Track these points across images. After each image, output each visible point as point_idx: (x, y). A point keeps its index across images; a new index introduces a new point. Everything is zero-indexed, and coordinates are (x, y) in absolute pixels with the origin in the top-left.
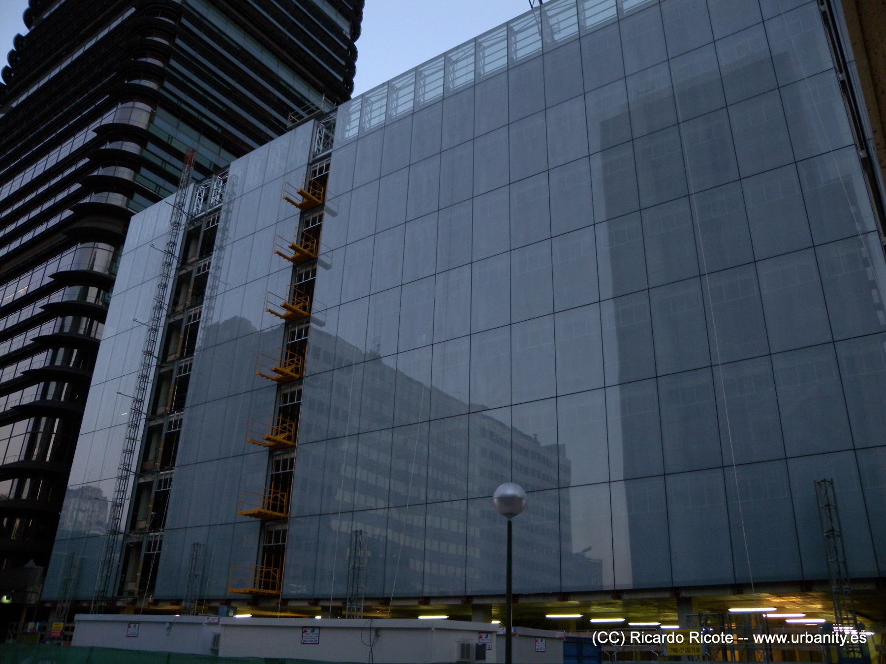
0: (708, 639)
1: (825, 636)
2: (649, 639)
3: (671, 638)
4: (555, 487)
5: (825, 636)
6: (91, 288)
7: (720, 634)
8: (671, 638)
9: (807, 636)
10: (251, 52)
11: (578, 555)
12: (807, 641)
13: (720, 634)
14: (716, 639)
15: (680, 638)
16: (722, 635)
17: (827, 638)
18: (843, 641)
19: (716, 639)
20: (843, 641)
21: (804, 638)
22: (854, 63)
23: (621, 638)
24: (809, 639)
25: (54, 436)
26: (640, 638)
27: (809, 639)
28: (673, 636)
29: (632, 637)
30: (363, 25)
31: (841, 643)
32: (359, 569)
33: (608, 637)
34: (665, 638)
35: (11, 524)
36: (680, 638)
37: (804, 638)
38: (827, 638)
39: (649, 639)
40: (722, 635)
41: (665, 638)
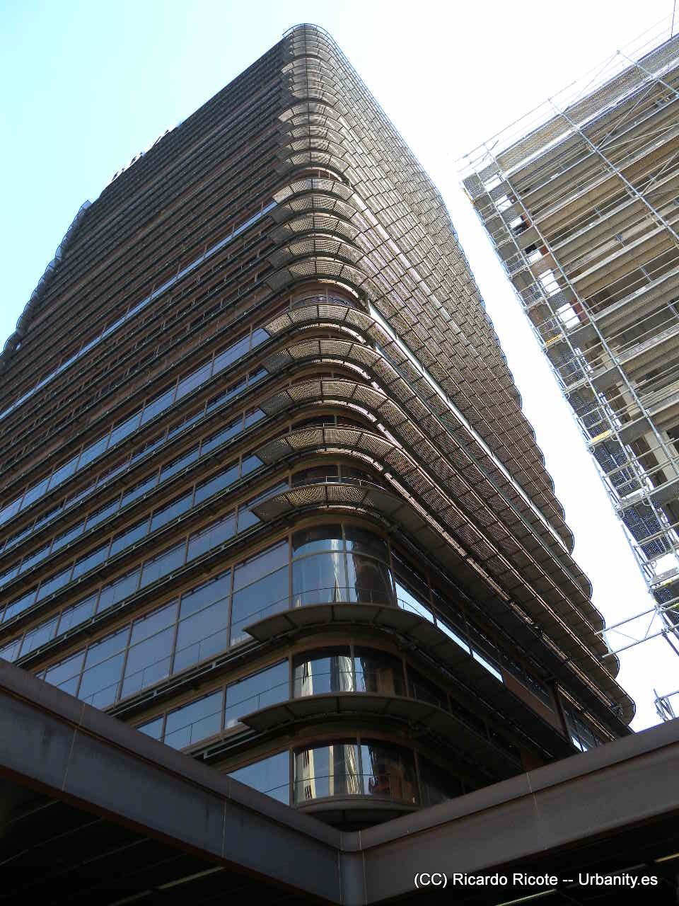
5: (615, 878)
6: (362, 687)
9: (597, 878)
10: (480, 281)
11: (285, 122)
12: (597, 883)
15: (503, 881)
16: (547, 877)
17: (617, 879)
18: (634, 883)
19: (437, 879)
20: (634, 883)
21: (594, 880)
31: (632, 885)
32: (73, 728)
33: (430, 879)
34: (489, 880)
36: (503, 881)
37: (594, 880)
38: (617, 879)
40: (547, 877)
41: (489, 880)
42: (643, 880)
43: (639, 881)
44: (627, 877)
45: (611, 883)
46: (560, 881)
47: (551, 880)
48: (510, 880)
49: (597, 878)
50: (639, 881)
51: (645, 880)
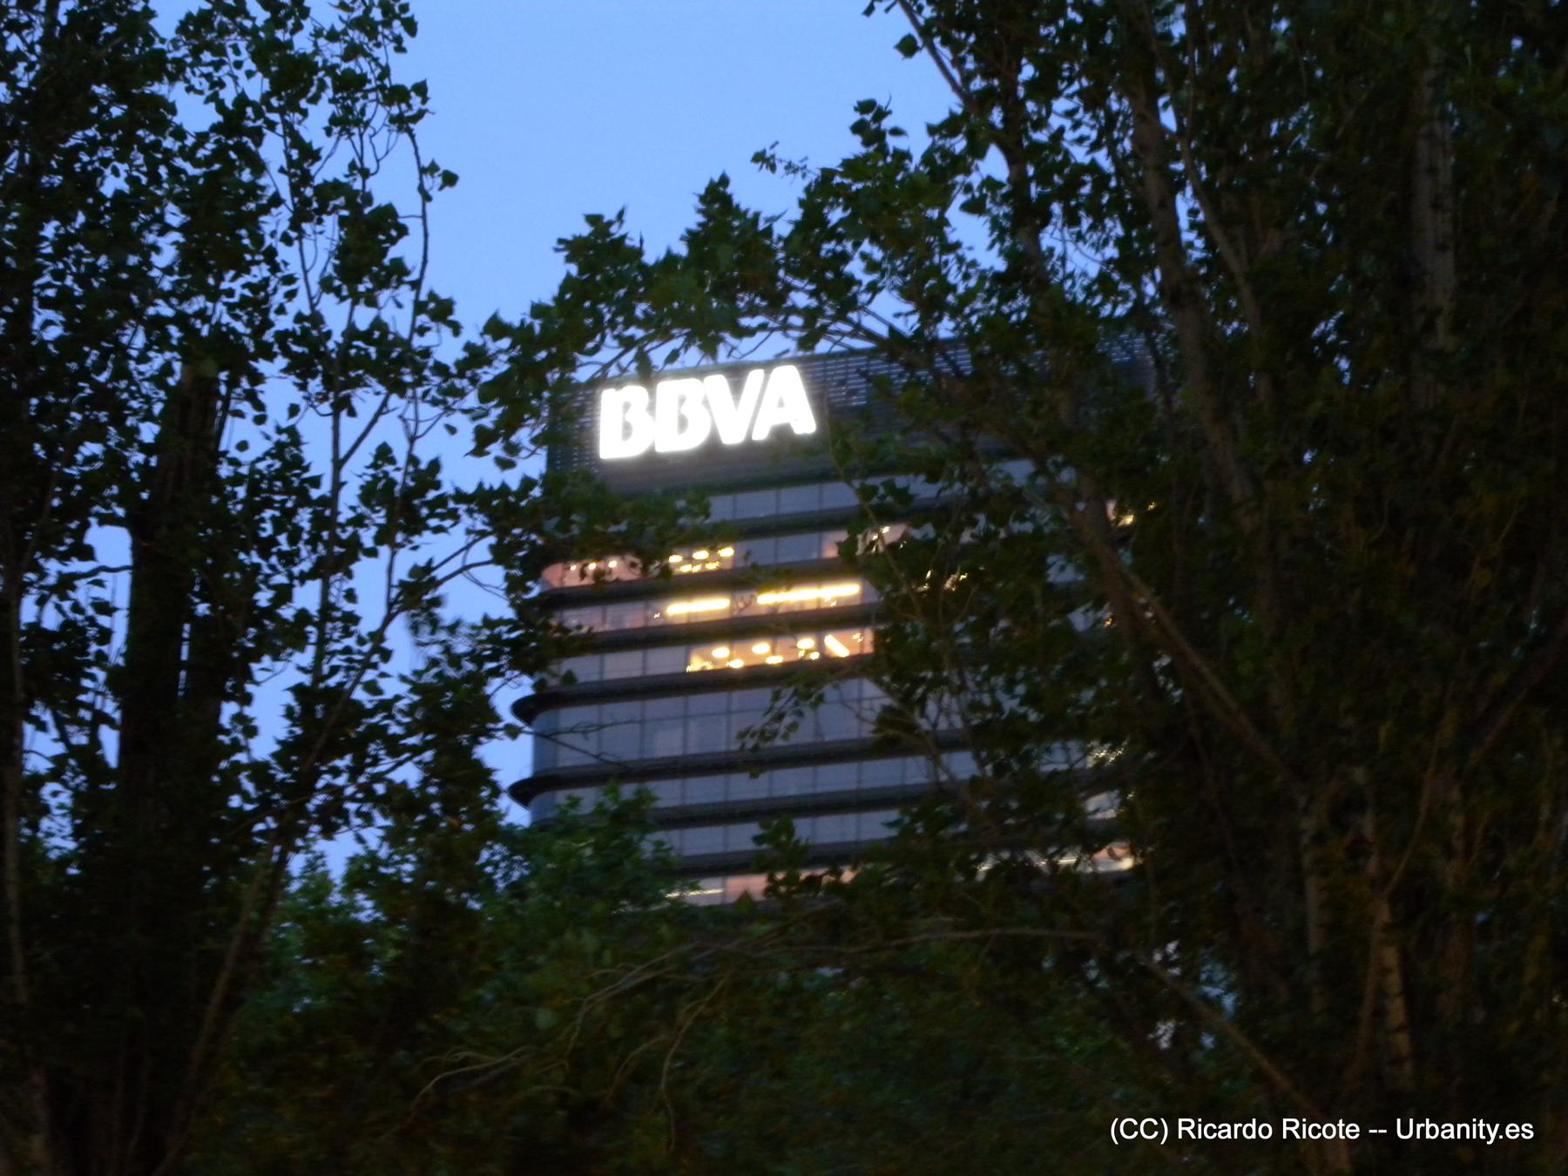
0: (1315, 1131)
1: (1459, 1126)
2: (1211, 1131)
3: (1249, 1131)
5: (1459, 1126)
7: (1336, 1124)
8: (1249, 1131)
9: (1428, 1126)
12: (1428, 1136)
13: (1336, 1124)
14: (1329, 1131)
15: (1265, 1131)
16: (1341, 1125)
17: (1463, 1129)
18: (1493, 1135)
19: (1329, 1131)
20: (1493, 1135)
21: (1423, 1130)
23: (1160, 1128)
24: (1432, 1131)
25: (1255, 1130)
26: (1299, 1131)
27: (1432, 1131)
28: (1253, 1126)
30: (429, 94)
31: (1488, 1138)
34: (1240, 1129)
36: (1265, 1131)
37: (1423, 1130)
38: (1463, 1129)
39: (1211, 1131)
40: (1341, 1125)
41: (1240, 1129)
42: (1508, 1131)
43: (1501, 1131)
44: (1481, 1125)
45: (1452, 1136)
47: (1348, 1131)
48: (1278, 1129)
49: (1428, 1126)
50: (1501, 1131)
51: (1512, 1131)
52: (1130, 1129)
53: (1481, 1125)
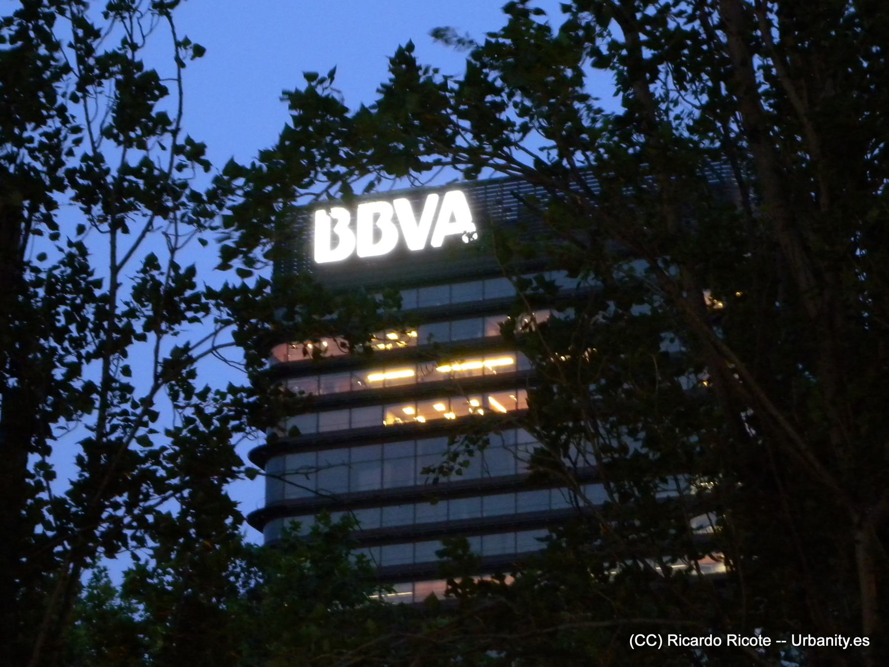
0: (746, 642)
1: (827, 639)
2: (686, 642)
3: (708, 642)
4: (413, 461)
5: (827, 639)
8: (708, 642)
12: (810, 644)
14: (754, 642)
15: (717, 642)
16: (760, 638)
17: (830, 641)
18: (846, 644)
19: (754, 642)
20: (846, 644)
21: (807, 641)
22: (755, 68)
23: (658, 640)
24: (812, 642)
27: (812, 642)
28: (711, 639)
29: (729, 640)
31: (844, 645)
34: (703, 641)
35: (708, 546)
36: (717, 642)
37: (807, 641)
38: (830, 641)
39: (686, 642)
40: (760, 638)
41: (703, 641)
42: (855, 641)
43: (851, 641)
44: (840, 638)
45: (823, 644)
46: (773, 642)
47: (764, 641)
50: (851, 641)
52: (641, 640)
53: (840, 638)
